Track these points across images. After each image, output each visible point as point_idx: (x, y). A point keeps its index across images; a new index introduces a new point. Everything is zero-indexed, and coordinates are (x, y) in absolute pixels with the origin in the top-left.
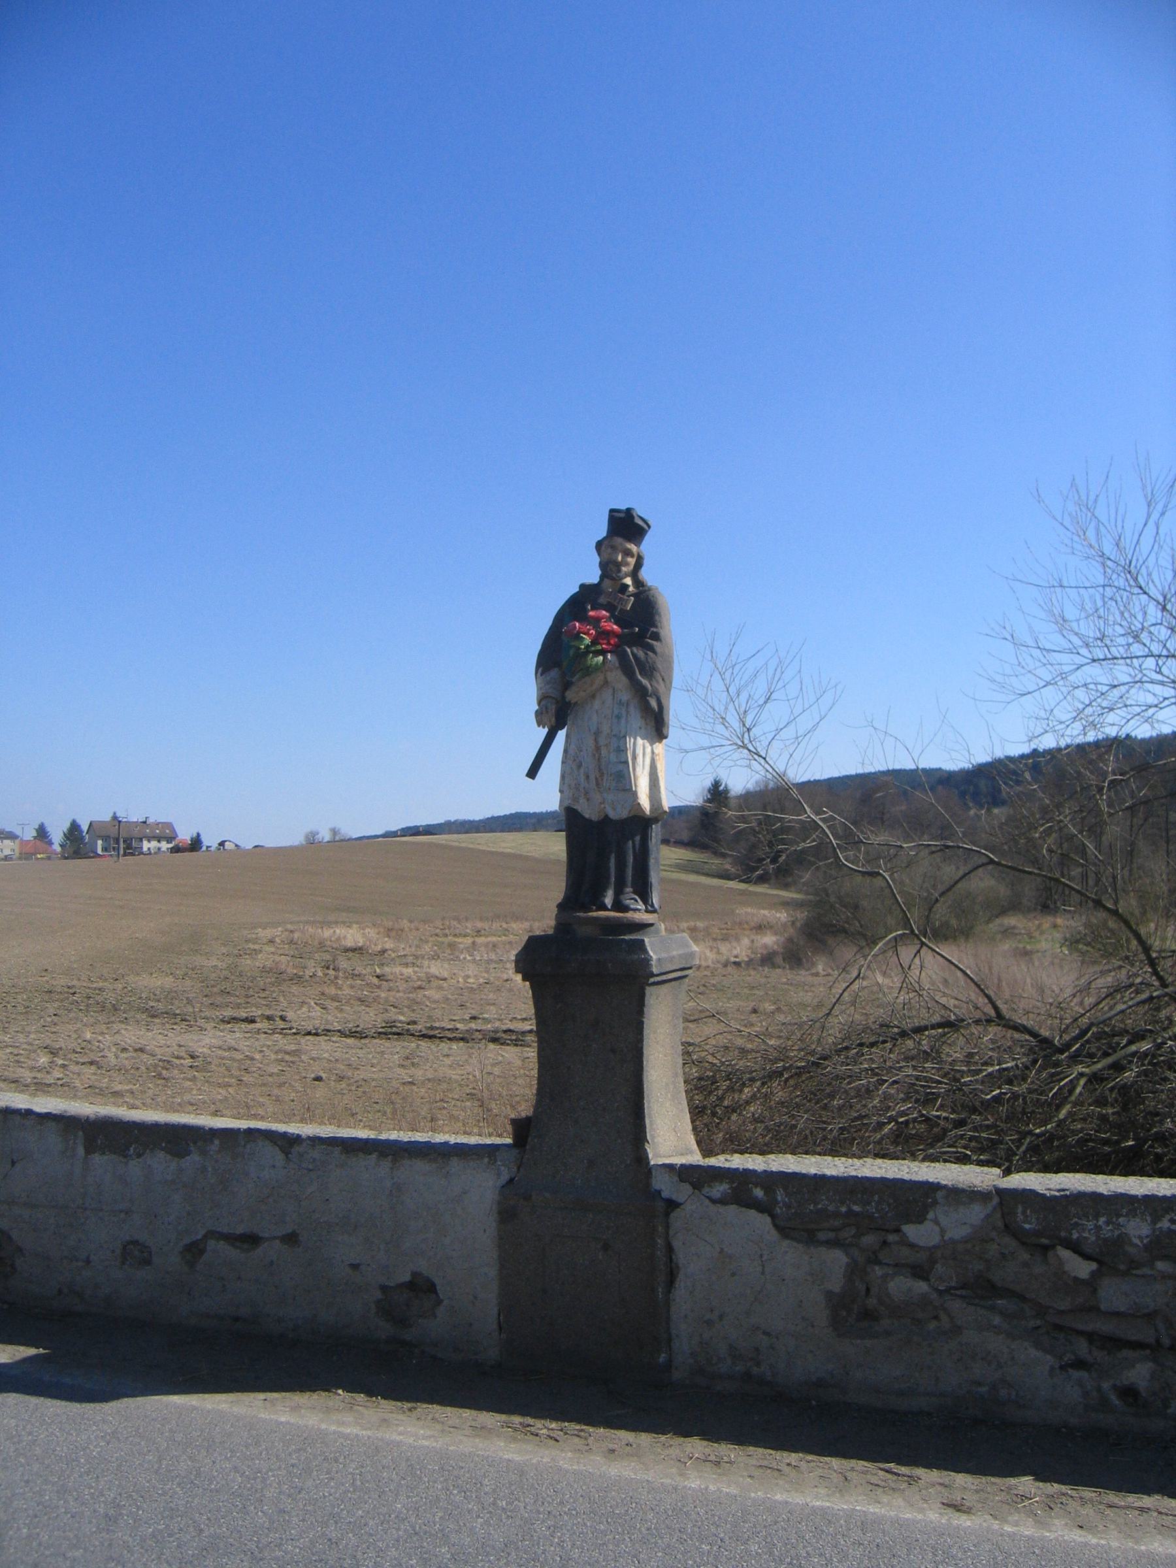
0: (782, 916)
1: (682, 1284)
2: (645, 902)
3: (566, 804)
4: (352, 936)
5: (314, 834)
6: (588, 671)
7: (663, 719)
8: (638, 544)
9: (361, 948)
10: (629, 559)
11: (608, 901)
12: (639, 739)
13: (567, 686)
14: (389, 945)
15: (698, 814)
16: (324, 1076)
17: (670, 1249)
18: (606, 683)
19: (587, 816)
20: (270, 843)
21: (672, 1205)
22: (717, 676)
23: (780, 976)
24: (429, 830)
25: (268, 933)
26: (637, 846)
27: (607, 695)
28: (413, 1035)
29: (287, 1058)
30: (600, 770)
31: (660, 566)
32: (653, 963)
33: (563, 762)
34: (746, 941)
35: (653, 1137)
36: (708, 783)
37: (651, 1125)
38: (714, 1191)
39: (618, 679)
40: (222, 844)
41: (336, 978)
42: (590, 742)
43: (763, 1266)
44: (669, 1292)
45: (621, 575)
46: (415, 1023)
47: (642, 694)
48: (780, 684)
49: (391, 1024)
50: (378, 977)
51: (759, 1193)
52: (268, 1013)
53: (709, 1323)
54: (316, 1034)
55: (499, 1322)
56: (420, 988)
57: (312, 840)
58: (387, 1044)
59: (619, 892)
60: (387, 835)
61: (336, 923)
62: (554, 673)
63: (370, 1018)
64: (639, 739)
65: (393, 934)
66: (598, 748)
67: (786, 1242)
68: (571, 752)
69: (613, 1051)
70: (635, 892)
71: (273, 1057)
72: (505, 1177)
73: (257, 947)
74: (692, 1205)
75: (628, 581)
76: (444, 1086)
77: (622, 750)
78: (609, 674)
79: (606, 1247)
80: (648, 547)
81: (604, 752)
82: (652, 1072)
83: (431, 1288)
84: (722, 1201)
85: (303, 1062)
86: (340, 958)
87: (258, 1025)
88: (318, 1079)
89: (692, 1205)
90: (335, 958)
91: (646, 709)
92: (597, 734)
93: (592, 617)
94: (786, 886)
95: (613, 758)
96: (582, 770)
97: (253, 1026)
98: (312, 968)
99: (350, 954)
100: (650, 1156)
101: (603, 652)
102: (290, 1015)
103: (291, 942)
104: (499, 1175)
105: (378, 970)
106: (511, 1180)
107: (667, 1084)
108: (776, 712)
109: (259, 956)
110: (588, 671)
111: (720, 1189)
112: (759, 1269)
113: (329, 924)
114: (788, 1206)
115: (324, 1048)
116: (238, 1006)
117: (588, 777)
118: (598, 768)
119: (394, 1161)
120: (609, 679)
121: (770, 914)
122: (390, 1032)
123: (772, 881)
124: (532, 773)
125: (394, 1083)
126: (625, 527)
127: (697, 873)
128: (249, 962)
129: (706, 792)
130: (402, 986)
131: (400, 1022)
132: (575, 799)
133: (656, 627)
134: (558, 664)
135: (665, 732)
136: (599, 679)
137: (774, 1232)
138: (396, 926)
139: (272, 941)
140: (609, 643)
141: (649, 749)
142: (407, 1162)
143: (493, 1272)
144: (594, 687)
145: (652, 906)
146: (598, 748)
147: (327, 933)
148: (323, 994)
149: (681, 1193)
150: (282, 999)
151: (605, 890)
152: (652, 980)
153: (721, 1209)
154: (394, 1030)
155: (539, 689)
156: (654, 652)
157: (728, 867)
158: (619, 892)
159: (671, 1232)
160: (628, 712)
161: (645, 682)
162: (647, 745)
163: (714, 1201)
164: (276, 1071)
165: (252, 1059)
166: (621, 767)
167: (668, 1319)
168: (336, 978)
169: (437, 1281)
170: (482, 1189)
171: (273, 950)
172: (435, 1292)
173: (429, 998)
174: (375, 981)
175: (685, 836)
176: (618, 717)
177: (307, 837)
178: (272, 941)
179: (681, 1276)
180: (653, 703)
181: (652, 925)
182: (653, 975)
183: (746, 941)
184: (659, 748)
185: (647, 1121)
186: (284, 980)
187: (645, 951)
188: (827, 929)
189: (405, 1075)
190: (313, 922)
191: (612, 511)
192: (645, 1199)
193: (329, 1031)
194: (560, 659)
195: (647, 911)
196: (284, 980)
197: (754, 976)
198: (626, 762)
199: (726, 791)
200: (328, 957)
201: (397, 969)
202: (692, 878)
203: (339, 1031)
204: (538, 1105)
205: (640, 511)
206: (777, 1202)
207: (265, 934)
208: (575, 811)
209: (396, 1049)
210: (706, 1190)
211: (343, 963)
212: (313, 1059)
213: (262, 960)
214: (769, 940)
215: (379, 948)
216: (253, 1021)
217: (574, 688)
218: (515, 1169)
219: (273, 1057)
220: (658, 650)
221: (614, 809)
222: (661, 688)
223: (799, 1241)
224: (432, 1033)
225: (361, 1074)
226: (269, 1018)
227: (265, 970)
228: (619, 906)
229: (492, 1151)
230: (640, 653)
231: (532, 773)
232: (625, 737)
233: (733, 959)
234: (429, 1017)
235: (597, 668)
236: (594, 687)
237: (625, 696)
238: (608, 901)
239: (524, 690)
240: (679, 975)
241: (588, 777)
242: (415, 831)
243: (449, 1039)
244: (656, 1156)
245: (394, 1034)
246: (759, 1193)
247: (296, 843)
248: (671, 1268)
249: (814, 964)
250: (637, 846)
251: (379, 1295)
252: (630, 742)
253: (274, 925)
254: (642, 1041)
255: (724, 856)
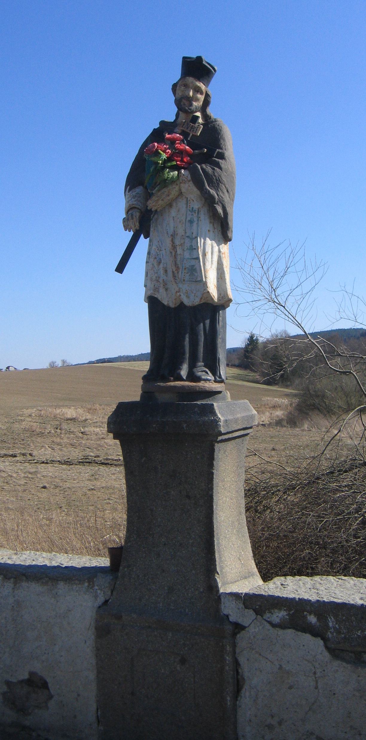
0: (285, 401)
1: (246, 696)
2: (214, 373)
3: (149, 293)
4: (70, 413)
5: (54, 363)
6: (166, 183)
7: (227, 224)
8: (207, 84)
9: (74, 419)
10: (199, 96)
11: (184, 373)
12: (208, 239)
13: (148, 196)
14: (89, 416)
15: (243, 351)
16: (47, 486)
17: (237, 663)
18: (181, 194)
19: (166, 303)
20: (31, 367)
21: (239, 627)
22: (256, 259)
23: (287, 431)
24: (110, 360)
25: (29, 411)
26: (207, 328)
27: (182, 204)
28: (97, 463)
29: (30, 476)
30: (176, 264)
31: (224, 103)
32: (221, 424)
33: (147, 262)
34: (267, 414)
35: (222, 568)
36: (248, 336)
37: (220, 558)
38: (275, 616)
39: (189, 189)
40: (8, 368)
41: (61, 433)
42: (168, 241)
43: (317, 682)
44: (237, 697)
45: (193, 108)
46: (98, 456)
47: (210, 202)
48: (292, 264)
49: (86, 457)
50: (82, 433)
51: (312, 619)
52: (23, 452)
53: (270, 727)
54: (47, 463)
55: (98, 716)
56: (103, 438)
57: (53, 366)
58: (83, 468)
59: (192, 366)
60: (90, 363)
61: (63, 406)
62: (139, 190)
63: (76, 454)
64: (208, 239)
65: (91, 411)
66: (174, 247)
67: (336, 663)
68: (152, 252)
69: (188, 497)
70: (205, 366)
71: (23, 475)
72: (101, 599)
73: (22, 418)
74: (255, 628)
75: (198, 114)
76: (111, 491)
77: (194, 248)
78: (182, 185)
79: (183, 661)
80: (214, 88)
81: (179, 251)
82: (221, 513)
83: (45, 685)
84: (281, 626)
85: (38, 478)
86: (64, 424)
87: (18, 458)
88: (44, 487)
89: (255, 628)
90: (60, 424)
91: (214, 215)
92: (173, 236)
93: (168, 139)
94: (287, 387)
95: (187, 255)
96: (161, 266)
97: (15, 459)
98: (49, 428)
99: (69, 422)
100: (220, 585)
101: (177, 168)
102: (35, 453)
103: (40, 416)
104: (96, 597)
105: (82, 430)
106: (106, 602)
107: (233, 522)
108: (291, 280)
109: (23, 423)
110: (166, 183)
111: (278, 615)
112: (313, 684)
113: (57, 407)
114: (339, 632)
115: (50, 470)
116: (9, 448)
117: (166, 271)
118: (176, 267)
119: (15, 583)
120: (183, 190)
121: (281, 400)
122: (86, 461)
123: (280, 383)
124: (120, 268)
125: (84, 489)
126: (196, 69)
127: (243, 380)
128: (18, 426)
129: (247, 340)
130: (93, 437)
131: (91, 456)
132: (156, 289)
133: (221, 149)
134: (141, 183)
135: (229, 235)
136: (174, 191)
137: (326, 654)
138: (94, 408)
139: (30, 416)
140: (182, 161)
141: (216, 249)
142: (24, 584)
143: (92, 676)
144: (171, 197)
145: (220, 377)
146: (174, 247)
147: (58, 411)
148: (53, 442)
149: (246, 617)
150: (32, 445)
151: (181, 363)
152: (220, 438)
153: (280, 632)
154: (87, 460)
155: (127, 202)
156: (220, 168)
157: (258, 377)
158: (192, 366)
159: (238, 651)
160: (199, 218)
161: (213, 192)
162: (215, 245)
163: (274, 626)
164: (23, 483)
165: (11, 476)
166: (193, 262)
167: (235, 724)
168: (61, 433)
169: (48, 680)
170: (81, 608)
171: (30, 419)
172: (48, 689)
173: (107, 444)
174: (81, 435)
175: (237, 362)
176: (191, 222)
177: (50, 364)
178: (30, 416)
179: (246, 687)
180: (220, 210)
181: (220, 392)
182: (221, 434)
183: (267, 414)
184: (225, 248)
185: (217, 555)
186: (35, 435)
187: (214, 414)
188: (310, 406)
189: (90, 485)
190: (52, 406)
191: (184, 58)
192: (215, 621)
193: (53, 461)
194: (144, 176)
195: (216, 381)
196: (35, 435)
197: (273, 431)
198: (198, 258)
199: (257, 340)
200: (58, 423)
201: (92, 429)
202: (240, 383)
203: (59, 461)
204: (128, 538)
205: (207, 59)
206: (328, 627)
207: (27, 412)
208: (156, 299)
209: (87, 471)
210: (267, 615)
211: (65, 426)
212: (43, 476)
213: (24, 425)
214: (279, 413)
215: (84, 418)
216: (15, 456)
217: (154, 198)
218: (109, 593)
219: (23, 475)
220: (223, 166)
221: (188, 297)
222: (226, 198)
223: (348, 662)
224: (106, 462)
225: (68, 485)
226: (24, 455)
227: (25, 430)
228: (193, 377)
229: (88, 574)
230: (209, 169)
231: (120, 268)
232: (196, 237)
233: (261, 423)
234: (106, 453)
235: (173, 181)
236: (171, 197)
237: (196, 205)
238: (184, 373)
239: (115, 202)
240: (243, 433)
241: (166, 271)
242: (103, 361)
243: (115, 465)
244: (224, 584)
245: (87, 462)
246: (312, 619)
247: (45, 367)
248: (238, 681)
249: (303, 425)
250: (207, 328)
251: (5, 688)
252: (200, 241)
253: (32, 407)
254: (212, 489)
255: (255, 372)
